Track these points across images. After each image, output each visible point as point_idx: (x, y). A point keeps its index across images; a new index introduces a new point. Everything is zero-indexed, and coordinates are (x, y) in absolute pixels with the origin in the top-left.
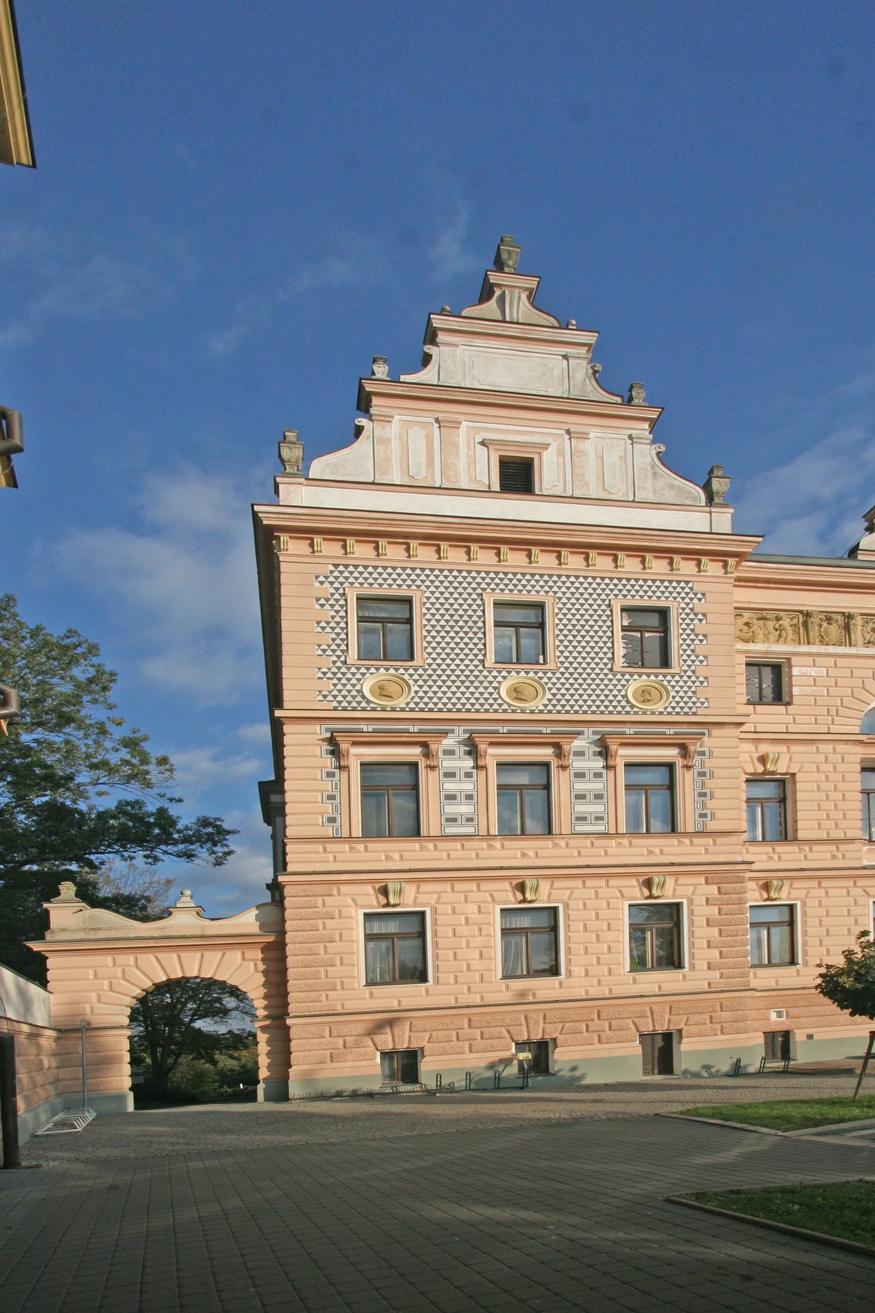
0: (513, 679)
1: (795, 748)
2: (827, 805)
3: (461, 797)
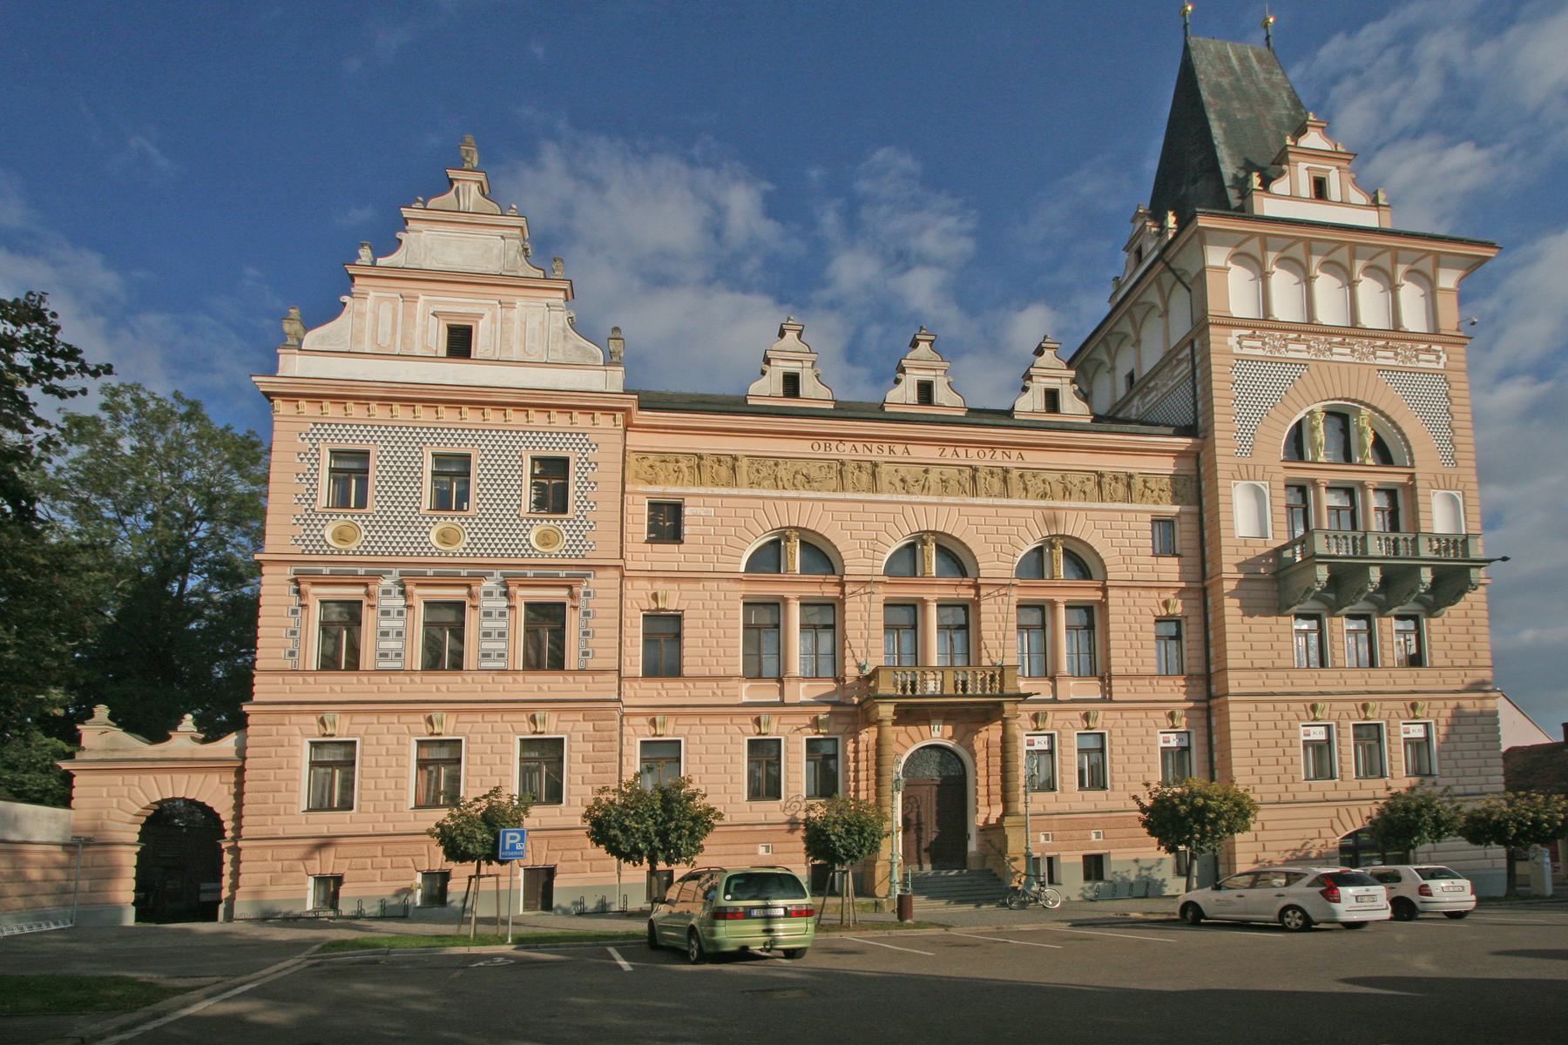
0: (442, 524)
1: (684, 586)
2: (1132, 653)
3: (393, 635)
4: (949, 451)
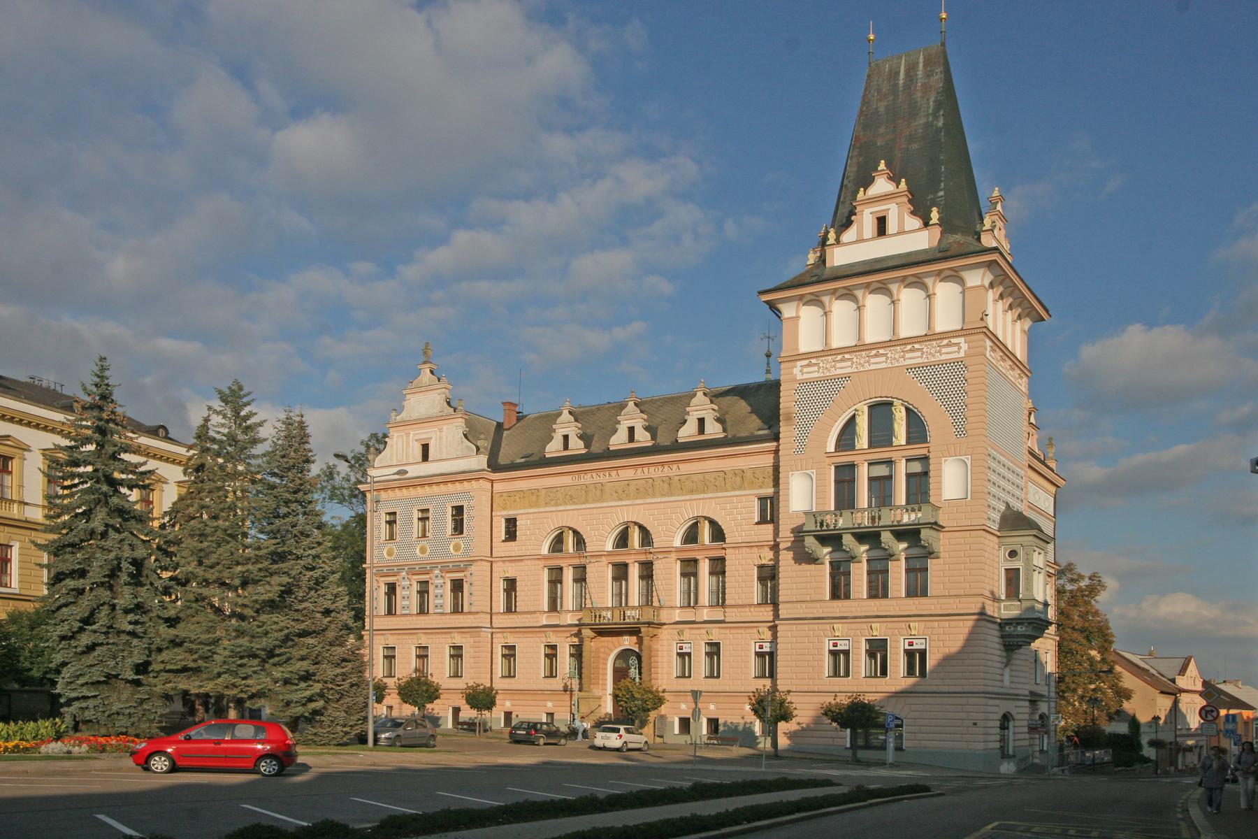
4: (640, 470)
